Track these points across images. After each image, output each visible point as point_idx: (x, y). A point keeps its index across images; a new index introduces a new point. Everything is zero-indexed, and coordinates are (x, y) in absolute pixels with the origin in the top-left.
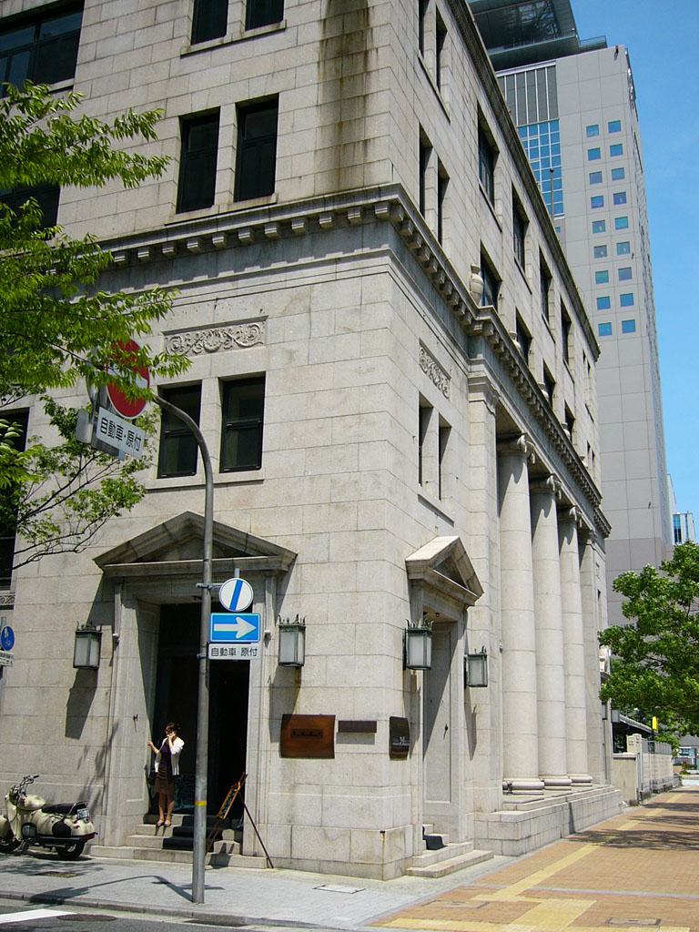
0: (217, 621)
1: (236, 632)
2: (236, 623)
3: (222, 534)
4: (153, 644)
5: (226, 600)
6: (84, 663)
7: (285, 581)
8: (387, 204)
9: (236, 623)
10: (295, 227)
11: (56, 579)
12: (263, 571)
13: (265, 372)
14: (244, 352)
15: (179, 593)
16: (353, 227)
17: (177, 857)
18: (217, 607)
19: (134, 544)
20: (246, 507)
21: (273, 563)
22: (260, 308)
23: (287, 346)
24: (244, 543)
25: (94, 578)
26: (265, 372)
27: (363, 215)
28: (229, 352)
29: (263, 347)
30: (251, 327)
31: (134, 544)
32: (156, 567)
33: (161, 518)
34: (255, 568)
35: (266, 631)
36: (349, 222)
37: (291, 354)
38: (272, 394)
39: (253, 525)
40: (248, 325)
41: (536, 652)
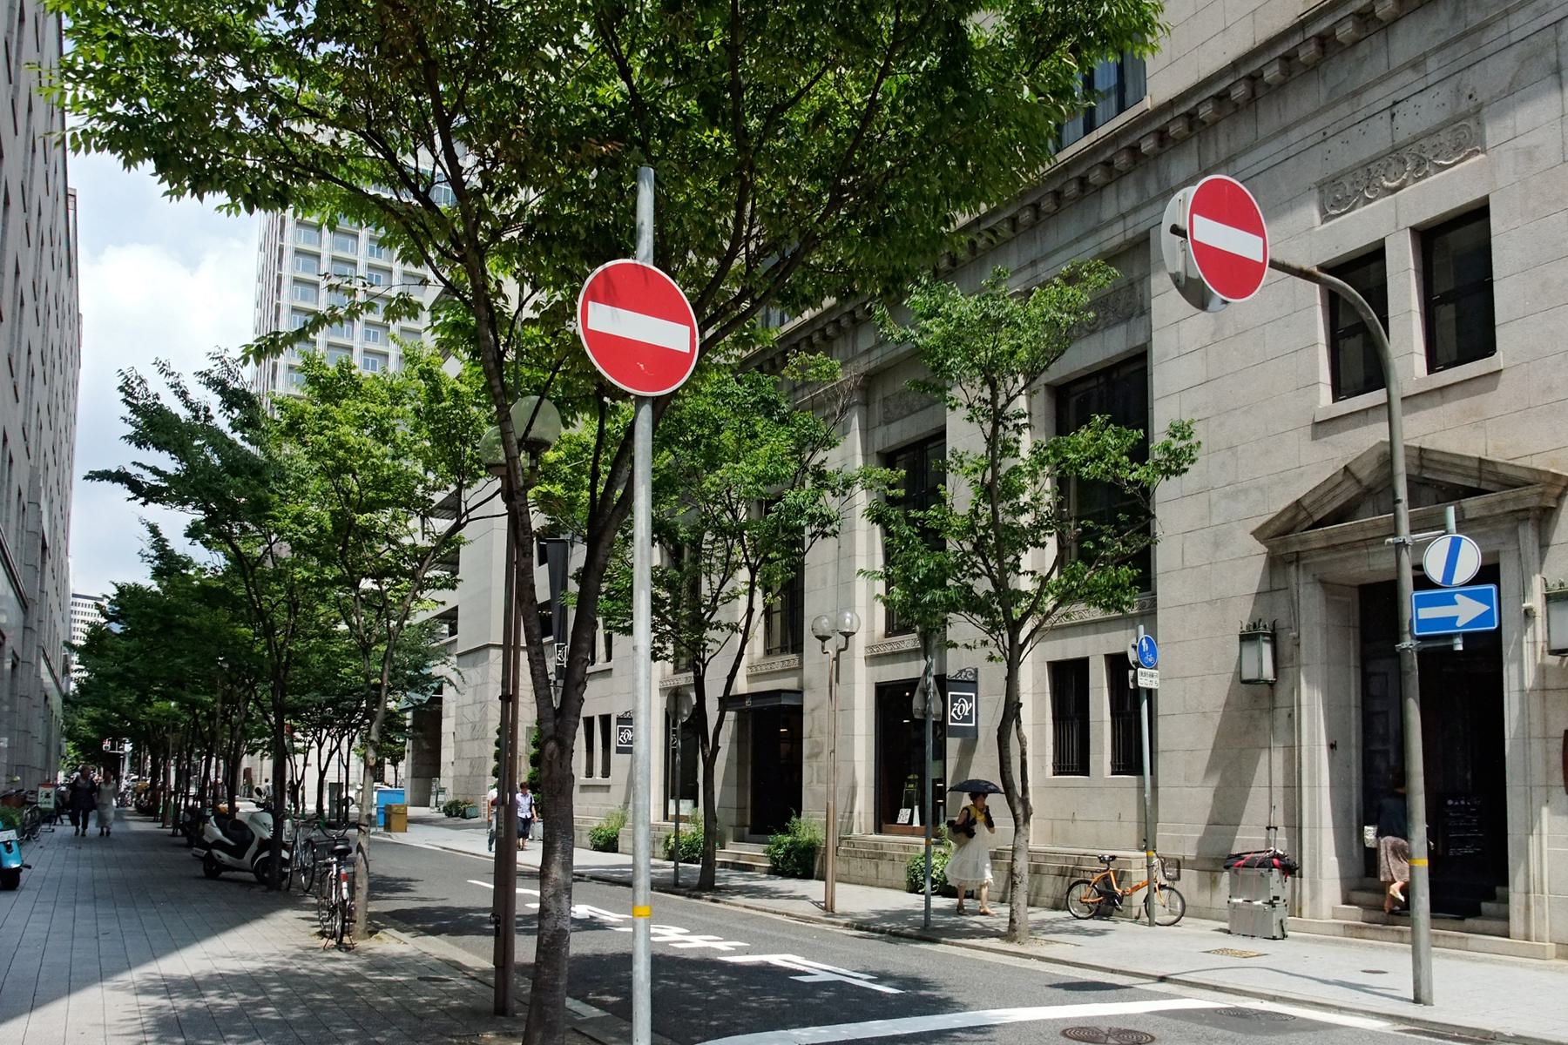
0: (1422, 603)
1: (1457, 617)
2: (1456, 603)
3: (1439, 467)
4: (1351, 642)
5: (1435, 572)
6: (1254, 676)
7: (1554, 518)
8: (650, 401)
9: (1456, 603)
10: (1172, 130)
11: (1207, 568)
12: (1514, 511)
13: (1487, 198)
14: (1448, 175)
15: (1376, 566)
16: (1312, 68)
17: (1471, 944)
18: (1422, 582)
19: (1306, 503)
20: (1475, 419)
21: (1529, 497)
22: (1468, 92)
23: (1522, 142)
24: (1475, 473)
25: (1257, 555)
26: (1487, 198)
27: (1357, 26)
28: (1424, 181)
29: (1482, 156)
30: (1455, 130)
31: (1306, 503)
32: (1343, 532)
33: (1343, 460)
34: (1498, 511)
35: (1526, 605)
36: (1268, 85)
37: (1530, 154)
38: (1503, 228)
39: (1490, 444)
40: (1450, 129)
41: (677, 885)
